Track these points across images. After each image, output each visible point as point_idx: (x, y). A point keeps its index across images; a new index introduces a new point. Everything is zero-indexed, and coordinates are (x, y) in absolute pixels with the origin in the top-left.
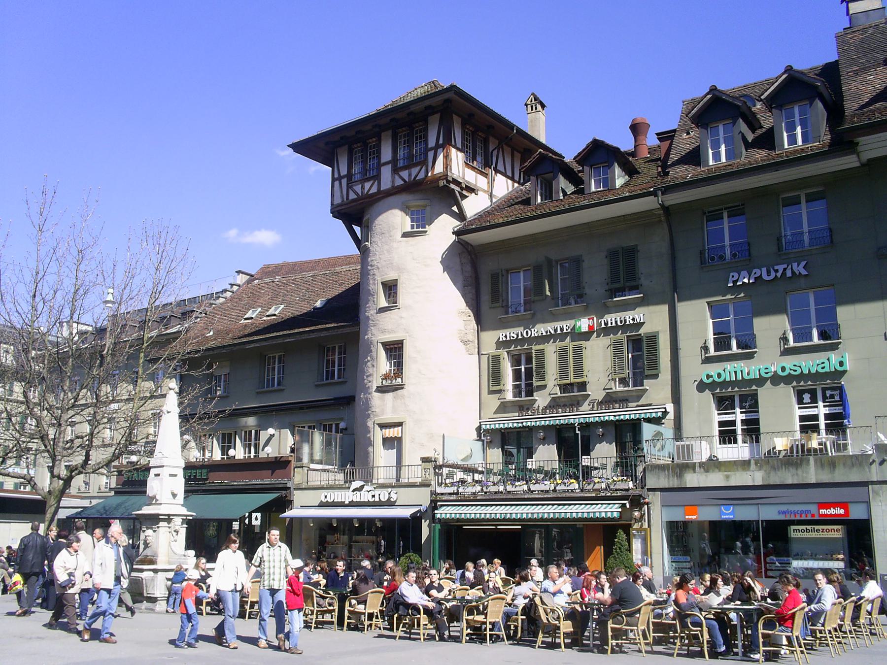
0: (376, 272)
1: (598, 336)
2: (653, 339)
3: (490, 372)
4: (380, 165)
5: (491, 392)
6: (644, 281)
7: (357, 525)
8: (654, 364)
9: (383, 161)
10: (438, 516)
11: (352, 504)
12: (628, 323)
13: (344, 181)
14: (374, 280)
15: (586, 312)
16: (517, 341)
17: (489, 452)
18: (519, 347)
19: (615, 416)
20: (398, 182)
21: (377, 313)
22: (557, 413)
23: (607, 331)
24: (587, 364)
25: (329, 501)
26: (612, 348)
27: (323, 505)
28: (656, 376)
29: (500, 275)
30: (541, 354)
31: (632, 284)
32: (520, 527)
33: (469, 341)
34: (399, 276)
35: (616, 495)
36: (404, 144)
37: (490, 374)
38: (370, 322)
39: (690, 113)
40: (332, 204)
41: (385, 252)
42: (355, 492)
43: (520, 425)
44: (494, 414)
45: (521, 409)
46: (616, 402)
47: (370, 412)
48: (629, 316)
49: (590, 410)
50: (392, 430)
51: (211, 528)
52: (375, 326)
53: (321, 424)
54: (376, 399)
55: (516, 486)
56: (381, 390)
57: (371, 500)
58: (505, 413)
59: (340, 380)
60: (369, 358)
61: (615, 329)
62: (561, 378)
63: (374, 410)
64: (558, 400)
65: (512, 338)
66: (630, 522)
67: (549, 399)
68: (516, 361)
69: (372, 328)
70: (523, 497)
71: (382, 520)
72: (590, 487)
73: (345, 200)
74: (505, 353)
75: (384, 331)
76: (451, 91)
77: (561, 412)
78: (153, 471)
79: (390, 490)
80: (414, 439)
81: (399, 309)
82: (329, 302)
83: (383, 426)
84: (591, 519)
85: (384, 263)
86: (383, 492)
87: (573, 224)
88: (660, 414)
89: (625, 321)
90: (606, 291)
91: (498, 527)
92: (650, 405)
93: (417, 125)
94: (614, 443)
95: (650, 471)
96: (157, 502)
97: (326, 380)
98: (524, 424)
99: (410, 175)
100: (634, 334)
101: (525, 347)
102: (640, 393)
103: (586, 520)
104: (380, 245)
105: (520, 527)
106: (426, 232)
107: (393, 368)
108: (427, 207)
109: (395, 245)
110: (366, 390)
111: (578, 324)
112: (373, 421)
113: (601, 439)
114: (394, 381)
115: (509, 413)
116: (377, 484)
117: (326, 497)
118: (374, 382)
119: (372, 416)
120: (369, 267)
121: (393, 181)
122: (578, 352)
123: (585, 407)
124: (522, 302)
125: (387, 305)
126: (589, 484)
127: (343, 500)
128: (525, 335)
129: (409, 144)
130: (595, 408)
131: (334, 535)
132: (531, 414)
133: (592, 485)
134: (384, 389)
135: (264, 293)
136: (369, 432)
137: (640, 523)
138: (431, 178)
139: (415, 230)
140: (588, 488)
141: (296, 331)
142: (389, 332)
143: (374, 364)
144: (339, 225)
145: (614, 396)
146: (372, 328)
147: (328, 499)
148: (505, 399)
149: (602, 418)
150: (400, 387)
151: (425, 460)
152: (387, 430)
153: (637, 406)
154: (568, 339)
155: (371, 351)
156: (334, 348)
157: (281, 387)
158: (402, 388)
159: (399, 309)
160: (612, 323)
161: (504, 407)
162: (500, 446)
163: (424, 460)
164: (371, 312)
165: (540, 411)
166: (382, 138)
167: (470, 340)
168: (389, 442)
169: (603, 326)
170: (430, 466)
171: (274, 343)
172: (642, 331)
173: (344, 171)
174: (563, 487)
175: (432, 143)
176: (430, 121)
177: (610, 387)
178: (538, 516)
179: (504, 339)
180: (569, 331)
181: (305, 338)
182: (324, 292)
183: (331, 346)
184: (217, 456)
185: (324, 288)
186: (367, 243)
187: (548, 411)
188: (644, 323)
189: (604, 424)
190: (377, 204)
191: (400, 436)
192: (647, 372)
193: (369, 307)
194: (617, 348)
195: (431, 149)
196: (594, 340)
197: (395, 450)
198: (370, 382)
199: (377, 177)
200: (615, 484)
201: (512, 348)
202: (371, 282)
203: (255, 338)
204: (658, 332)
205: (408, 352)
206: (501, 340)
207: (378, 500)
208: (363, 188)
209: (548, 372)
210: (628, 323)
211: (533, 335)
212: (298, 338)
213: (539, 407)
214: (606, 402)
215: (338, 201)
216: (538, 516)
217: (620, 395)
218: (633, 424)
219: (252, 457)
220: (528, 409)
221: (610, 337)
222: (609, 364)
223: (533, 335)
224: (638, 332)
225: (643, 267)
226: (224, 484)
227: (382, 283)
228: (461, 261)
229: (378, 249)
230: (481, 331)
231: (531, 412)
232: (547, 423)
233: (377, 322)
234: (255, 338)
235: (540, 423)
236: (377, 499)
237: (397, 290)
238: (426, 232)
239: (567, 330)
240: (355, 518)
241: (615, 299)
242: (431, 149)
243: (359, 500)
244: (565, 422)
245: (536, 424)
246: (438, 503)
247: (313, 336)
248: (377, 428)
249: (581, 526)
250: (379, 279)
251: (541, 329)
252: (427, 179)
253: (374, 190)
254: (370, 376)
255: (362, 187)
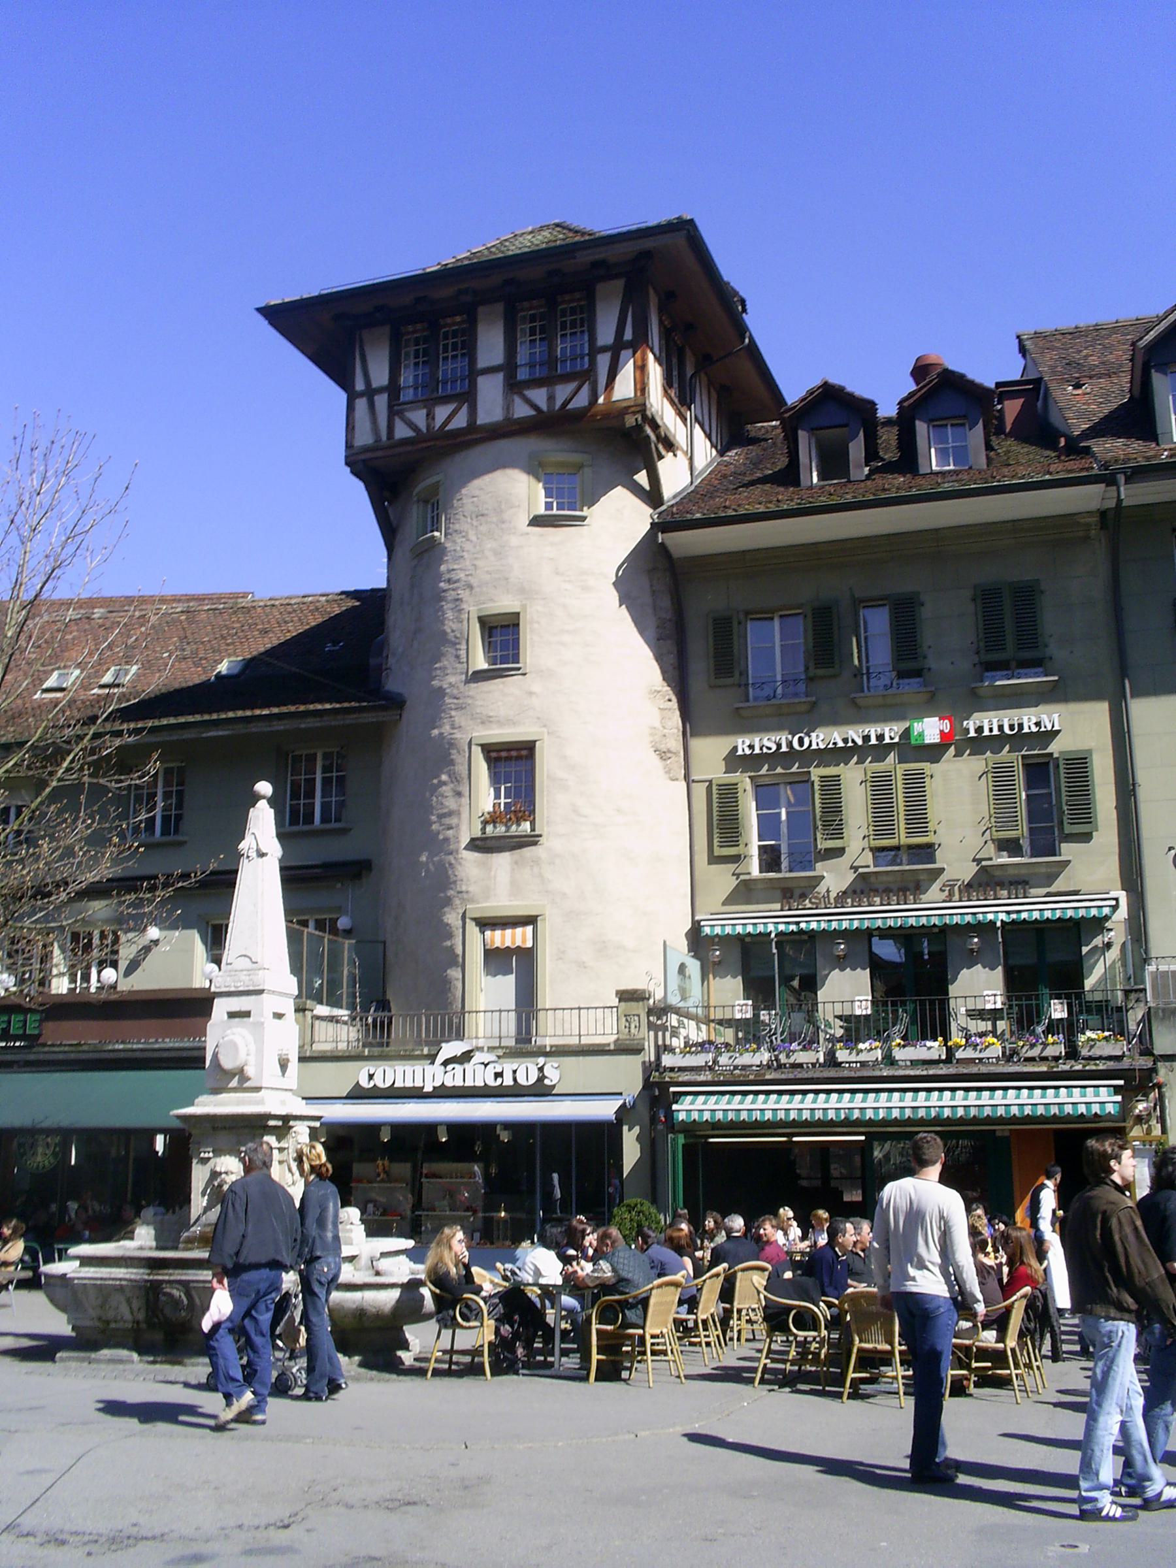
0: (464, 594)
1: (959, 754)
2: (1079, 764)
3: (715, 818)
4: (473, 374)
5: (714, 860)
6: (1054, 650)
7: (444, 1140)
8: (1084, 812)
9: (482, 363)
10: (682, 1116)
11: (443, 1093)
12: (1026, 730)
13: (382, 401)
14: (460, 611)
15: (930, 706)
16: (775, 757)
17: (715, 983)
18: (779, 770)
19: (1008, 913)
20: (522, 411)
21: (467, 682)
22: (870, 905)
23: (980, 744)
24: (936, 809)
25: (381, 1085)
26: (990, 779)
27: (358, 1094)
28: (1086, 837)
29: (735, 623)
30: (832, 786)
31: (1027, 655)
32: (863, 1138)
33: (669, 751)
34: (524, 607)
35: (1094, 1068)
36: (417, 357)
37: (715, 823)
38: (448, 700)
39: (1141, 338)
40: (349, 445)
41: (487, 553)
42: (450, 1067)
43: (793, 927)
44: (724, 904)
45: (788, 895)
46: (1001, 885)
47: (451, 893)
48: (1028, 719)
49: (944, 901)
50: (509, 932)
51: (40, 1150)
52: (462, 708)
53: (207, 923)
54: (470, 866)
55: (859, 1052)
56: (481, 845)
57: (491, 1082)
58: (748, 902)
59: (166, 839)
60: (444, 777)
61: (996, 742)
62: (878, 834)
63: (464, 888)
64: (873, 879)
65: (765, 750)
66: (1123, 1124)
67: (851, 877)
68: (765, 795)
69: (453, 713)
70: (877, 1073)
71: (509, 1125)
72: (1035, 1052)
73: (384, 438)
74: (748, 780)
75: (486, 721)
76: (679, 230)
77: (895, 902)
78: (221, 1008)
79: (541, 1060)
80: (563, 952)
81: (524, 674)
82: (250, 664)
83: (485, 924)
84: (1029, 1119)
85: (487, 577)
86: (523, 1067)
87: (728, 550)
88: (1106, 911)
89: (1021, 726)
90: (975, 665)
91: (795, 1139)
92: (1076, 893)
93: (410, 328)
94: (868, 970)
95: (1163, 1019)
96: (247, 1085)
97: (291, 824)
98: (803, 925)
99: (551, 398)
100: (1036, 752)
101: (794, 769)
102: (1055, 870)
103: (1014, 1120)
104: (474, 538)
105: (863, 1138)
106: (584, 519)
107: (503, 801)
108: (586, 470)
109: (514, 541)
110: (441, 846)
111: (917, 727)
112: (461, 911)
113: (971, 959)
114: (514, 827)
115: (758, 903)
116: (500, 1047)
117: (371, 1077)
118: (464, 828)
119: (457, 902)
120: (442, 585)
121: (508, 407)
122: (916, 784)
123: (934, 893)
124: (779, 678)
125: (485, 666)
126: (1032, 1046)
127: (419, 1084)
128: (796, 745)
129: (546, 333)
130: (957, 897)
131: (376, 1161)
132: (809, 906)
133: (1040, 1048)
134: (489, 844)
135: (73, 639)
136: (450, 936)
137: (1145, 1127)
138: (603, 408)
139: (555, 512)
140: (1030, 1054)
141: (165, 722)
142: (500, 724)
143: (460, 789)
144: (357, 493)
145: (998, 873)
146: (453, 713)
147: (378, 1081)
148: (749, 873)
149: (980, 917)
150: (532, 840)
151: (626, 996)
152: (498, 933)
153: (1048, 895)
154: (891, 758)
155: (452, 763)
156: (312, 759)
157: (180, 838)
158: (535, 843)
159: (525, 674)
160: (991, 730)
161: (745, 892)
162: (740, 970)
163: (624, 996)
164: (452, 679)
165: (832, 901)
166: (479, 317)
167: (673, 749)
168: (496, 959)
169: (972, 734)
170: (640, 1009)
171: (175, 738)
172: (1055, 748)
173: (380, 375)
174: (969, 1053)
175: (606, 334)
176: (598, 295)
177: (987, 856)
178: (928, 1114)
179: (748, 752)
180: (896, 740)
181: (259, 730)
182: (228, 645)
183: (304, 752)
184: (61, 986)
185: (223, 637)
186: (436, 534)
187: (849, 900)
188: (1058, 732)
189: (985, 929)
190: (464, 454)
191: (529, 944)
192: (1068, 829)
193: (443, 668)
194: (1000, 778)
195: (604, 349)
196: (948, 761)
197: (511, 979)
198: (450, 828)
199: (468, 397)
200: (1092, 1047)
201: (764, 771)
202: (450, 615)
203: (863, 649)
204: (1090, 751)
205: (547, 764)
206: (740, 752)
207: (511, 1083)
208: (430, 416)
209: (850, 822)
210: (1026, 730)
211: (814, 746)
212: (241, 729)
213: (828, 891)
214: (980, 885)
215: (364, 438)
216: (928, 1114)
217: (1011, 871)
218: (1037, 930)
219: (93, 990)
220: (803, 896)
221: (985, 756)
222: (984, 809)
223: (814, 746)
224: (1045, 749)
225: (1051, 622)
226: (85, 1048)
227: (482, 620)
228: (651, 586)
229: (467, 546)
230: (691, 736)
231: (810, 902)
232: (856, 924)
233: (470, 701)
234: (863, 649)
235: (840, 925)
236: (508, 1081)
237: (518, 634)
238: (584, 519)
239: (891, 738)
240: (440, 1124)
241: (998, 683)
242: (604, 349)
243: (461, 1084)
244: (896, 923)
245: (830, 926)
246: (672, 1089)
247: (279, 726)
248: (472, 929)
249: (1007, 1134)
250: (473, 608)
251: (819, 739)
252: (593, 410)
253: (460, 421)
254: (450, 814)
255: (428, 415)
